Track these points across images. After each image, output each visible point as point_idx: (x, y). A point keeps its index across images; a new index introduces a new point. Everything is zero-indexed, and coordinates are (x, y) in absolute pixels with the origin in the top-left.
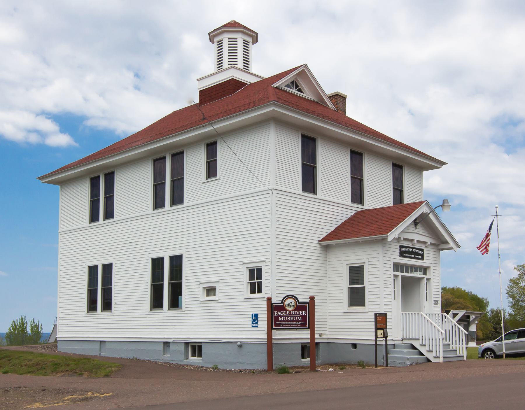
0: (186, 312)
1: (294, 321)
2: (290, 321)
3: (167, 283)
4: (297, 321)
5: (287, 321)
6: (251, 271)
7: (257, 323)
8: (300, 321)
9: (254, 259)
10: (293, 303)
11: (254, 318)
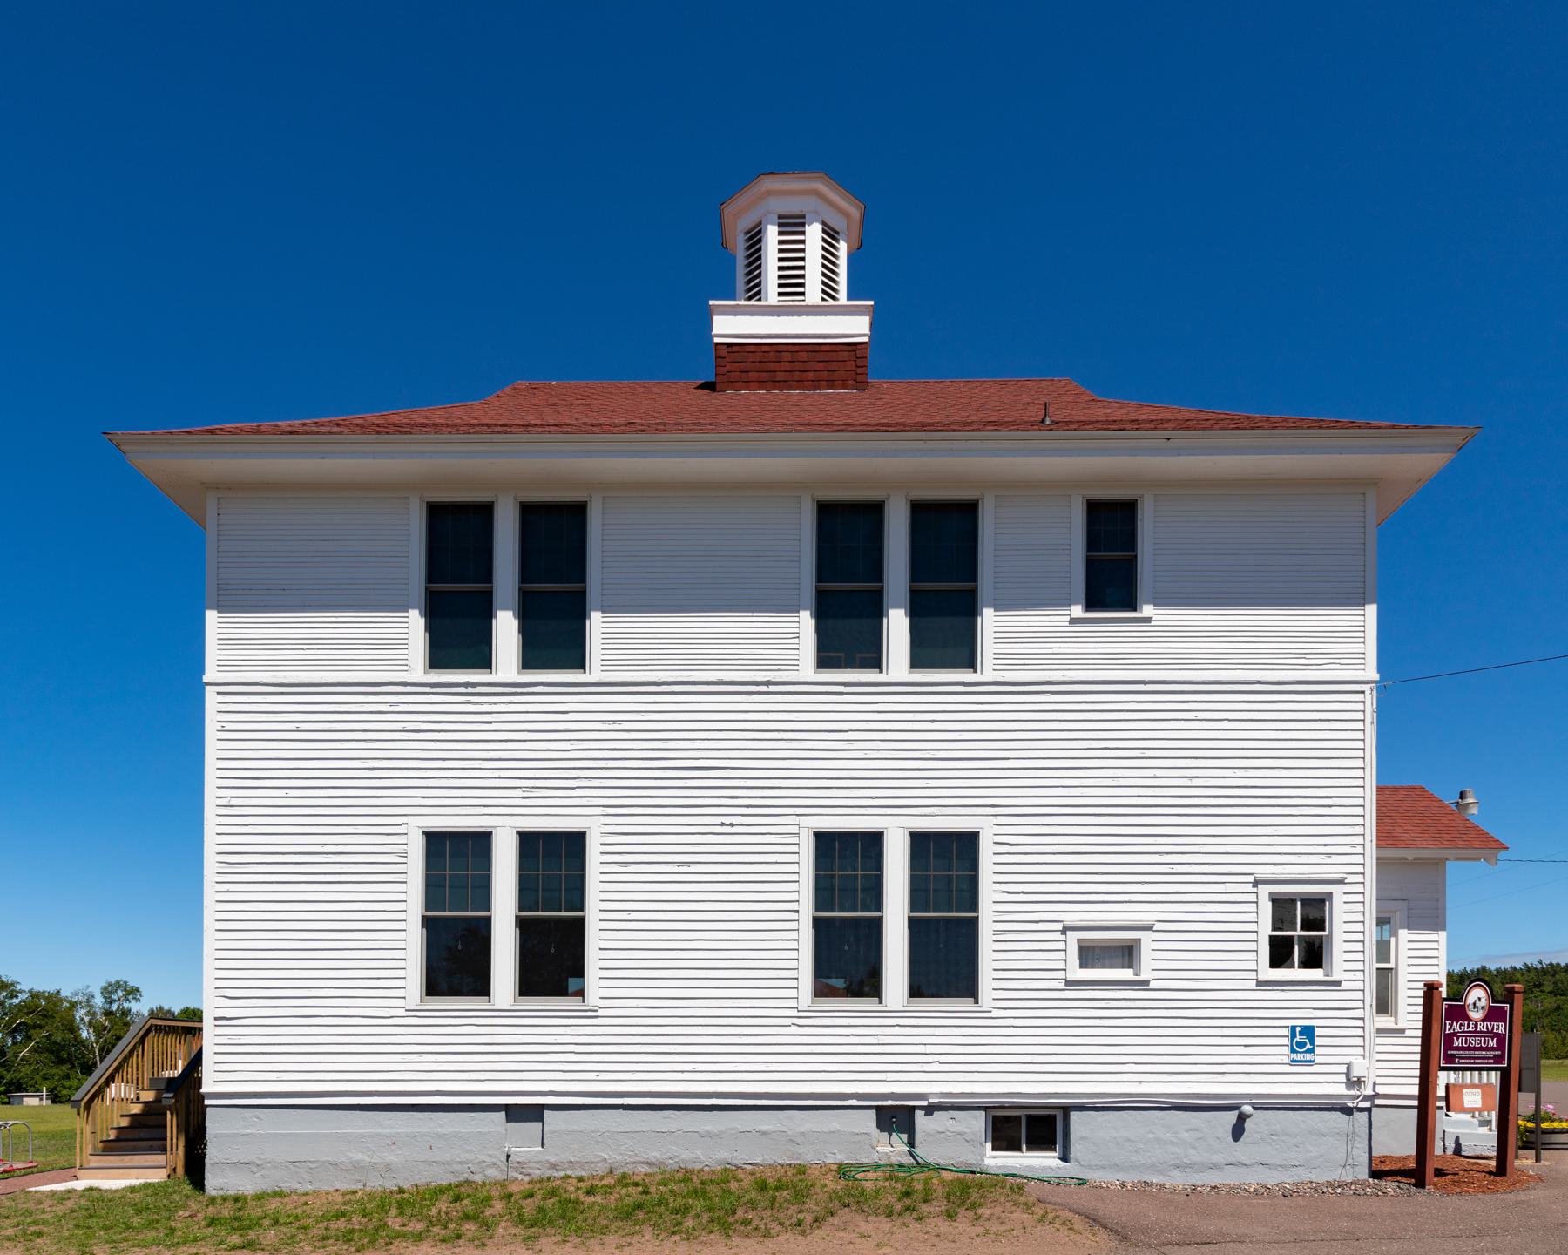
0: (995, 1013)
1: (1481, 1049)
2: (1475, 1049)
3: (896, 914)
4: (1487, 1049)
5: (1469, 1048)
6: (1282, 907)
7: (1311, 1051)
8: (1492, 1049)
9: (1299, 869)
10: (1484, 1002)
11: (1298, 1038)
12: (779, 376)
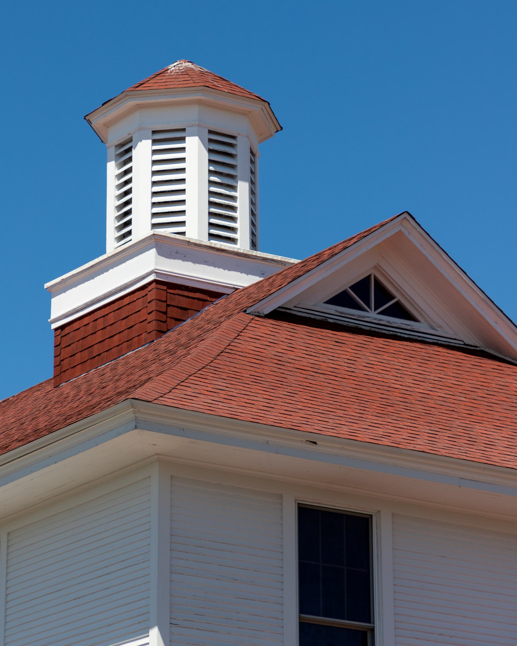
12: (96, 350)
